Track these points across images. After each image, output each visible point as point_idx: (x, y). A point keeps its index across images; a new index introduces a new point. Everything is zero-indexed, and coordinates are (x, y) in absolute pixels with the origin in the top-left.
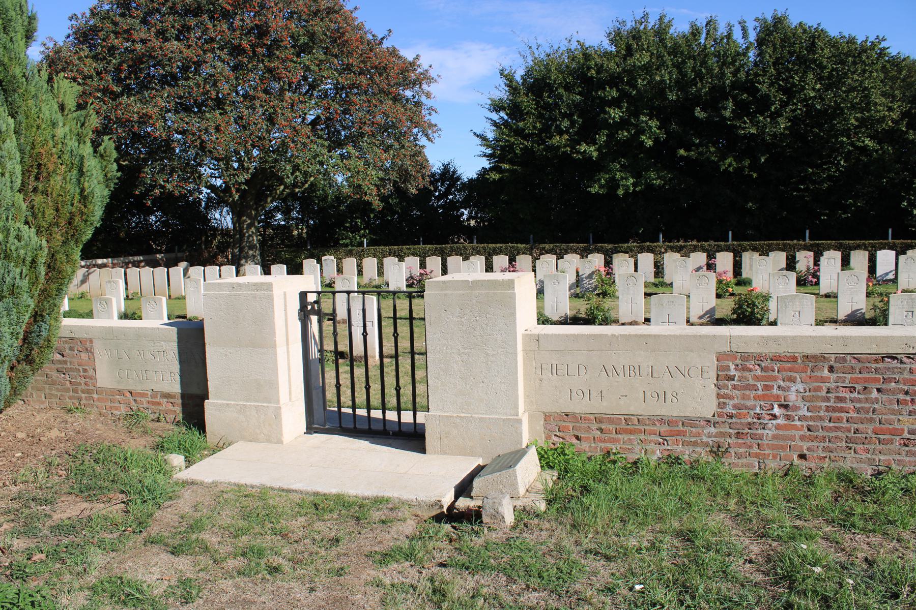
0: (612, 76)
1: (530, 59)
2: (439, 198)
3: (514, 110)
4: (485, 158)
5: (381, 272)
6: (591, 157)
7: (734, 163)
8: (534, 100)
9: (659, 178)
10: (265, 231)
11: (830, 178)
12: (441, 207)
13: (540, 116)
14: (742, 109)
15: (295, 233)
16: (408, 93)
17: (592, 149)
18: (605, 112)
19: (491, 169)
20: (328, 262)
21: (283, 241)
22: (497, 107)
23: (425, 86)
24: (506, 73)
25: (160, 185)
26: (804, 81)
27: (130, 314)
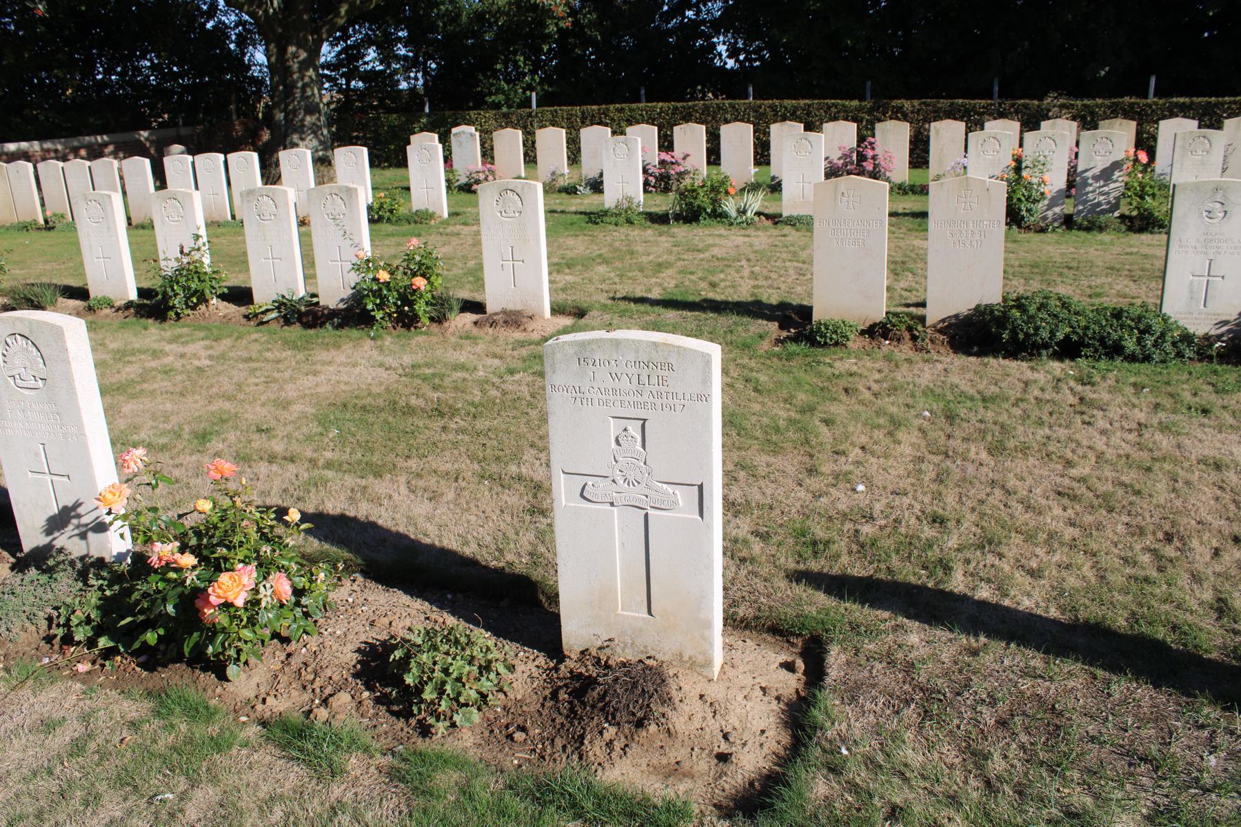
5: (574, 156)
10: (348, 84)
15: (404, 85)
20: (463, 138)
21: (381, 101)
27: (404, 222)
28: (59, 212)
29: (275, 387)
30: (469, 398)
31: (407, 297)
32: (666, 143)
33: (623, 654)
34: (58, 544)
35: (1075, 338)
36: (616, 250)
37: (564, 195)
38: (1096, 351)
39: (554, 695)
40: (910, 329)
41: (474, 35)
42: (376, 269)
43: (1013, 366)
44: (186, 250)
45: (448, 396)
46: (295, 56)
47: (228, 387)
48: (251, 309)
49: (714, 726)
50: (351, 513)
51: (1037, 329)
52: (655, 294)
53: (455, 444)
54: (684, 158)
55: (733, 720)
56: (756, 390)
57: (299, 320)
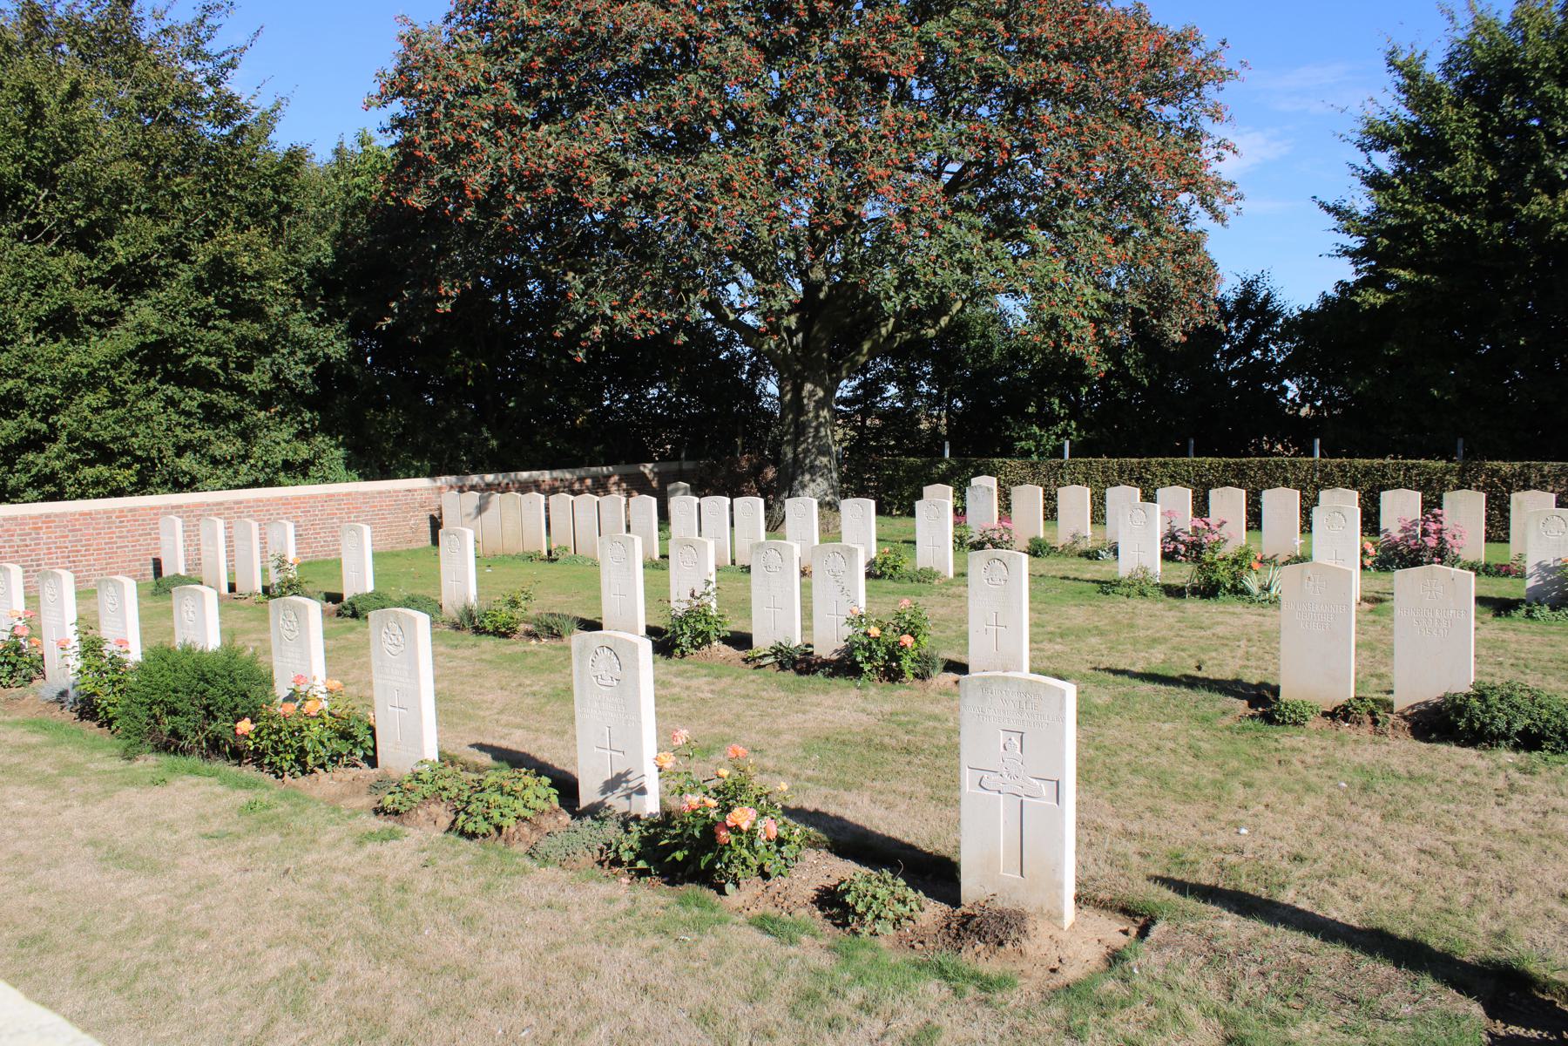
1: (1464, 19)
2: (1230, 356)
3: (1421, 147)
4: (1347, 259)
5: (1098, 516)
8: (1475, 115)
10: (863, 421)
12: (1236, 373)
15: (924, 425)
16: (1170, 112)
19: (1362, 284)
22: (1380, 138)
24: (1400, 59)
25: (604, 315)
28: (563, 545)
29: (768, 719)
30: (935, 742)
31: (894, 653)
33: (1000, 904)
34: (609, 802)
35: (1534, 730)
36: (1117, 622)
37: (1084, 560)
38: (1558, 745)
39: (948, 926)
40: (1372, 713)
41: (1007, 373)
42: (868, 625)
43: (1468, 755)
44: (697, 594)
45: (917, 739)
46: (812, 394)
47: (728, 716)
48: (750, 653)
49: (1054, 954)
50: (823, 809)
51: (1493, 718)
52: (1138, 668)
53: (915, 775)
55: (1070, 952)
56: (1196, 756)
57: (794, 666)
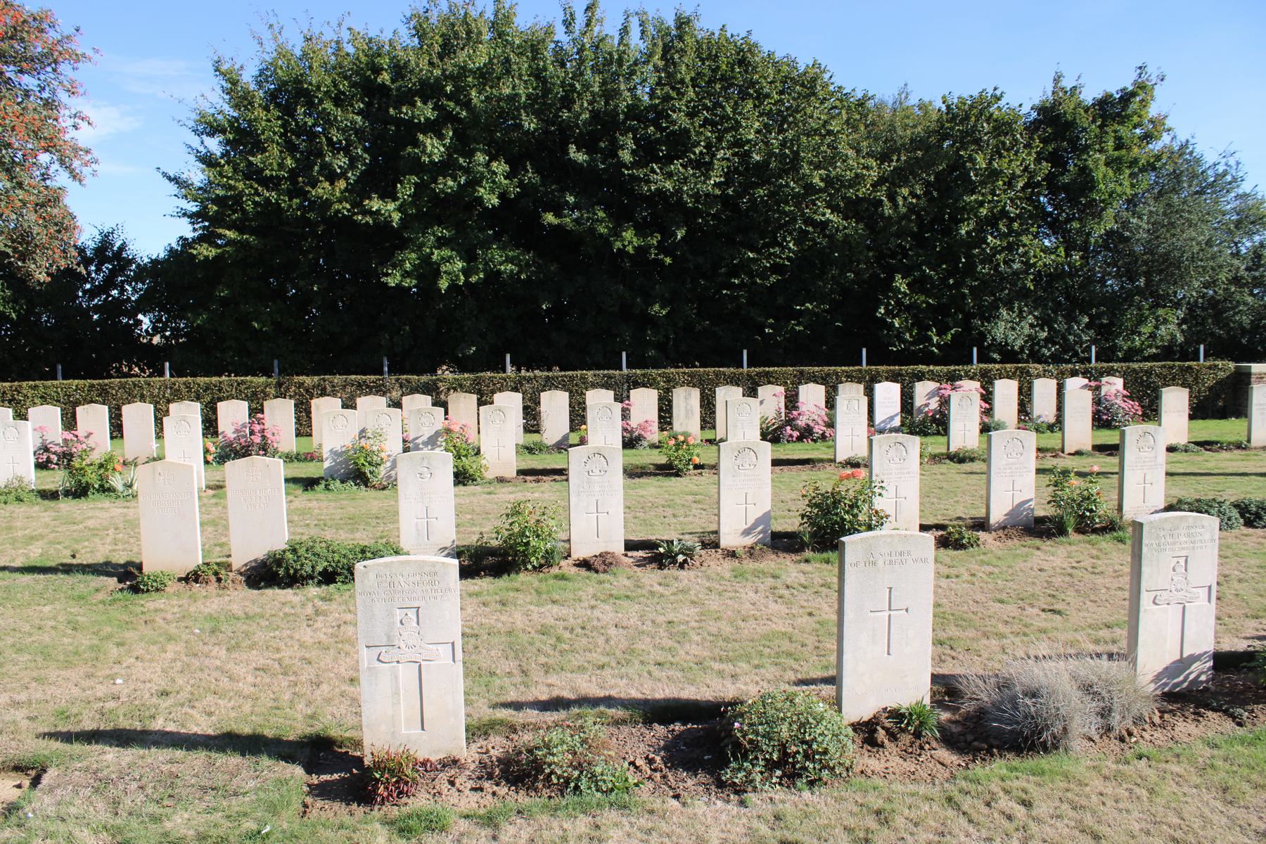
0: (423, 83)
1: (270, 46)
3: (242, 138)
4: (186, 220)
6: (388, 222)
7: (635, 239)
8: (279, 118)
9: (509, 260)
11: (776, 269)
12: (97, 309)
13: (290, 148)
14: (646, 153)
16: (28, 81)
17: (391, 206)
18: (416, 143)
19: (200, 239)
23: (64, 68)
26: (740, 114)
32: (70, 422)
35: (330, 569)
40: (216, 574)
51: (302, 565)
54: (87, 437)
